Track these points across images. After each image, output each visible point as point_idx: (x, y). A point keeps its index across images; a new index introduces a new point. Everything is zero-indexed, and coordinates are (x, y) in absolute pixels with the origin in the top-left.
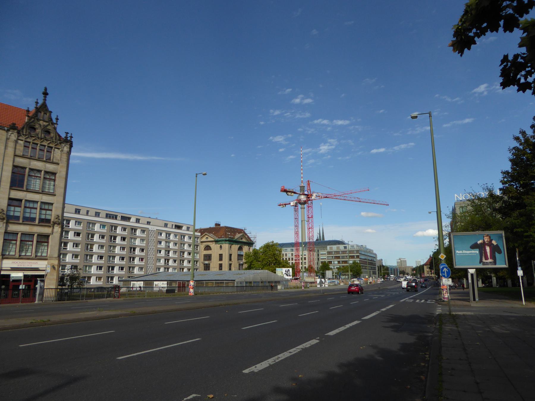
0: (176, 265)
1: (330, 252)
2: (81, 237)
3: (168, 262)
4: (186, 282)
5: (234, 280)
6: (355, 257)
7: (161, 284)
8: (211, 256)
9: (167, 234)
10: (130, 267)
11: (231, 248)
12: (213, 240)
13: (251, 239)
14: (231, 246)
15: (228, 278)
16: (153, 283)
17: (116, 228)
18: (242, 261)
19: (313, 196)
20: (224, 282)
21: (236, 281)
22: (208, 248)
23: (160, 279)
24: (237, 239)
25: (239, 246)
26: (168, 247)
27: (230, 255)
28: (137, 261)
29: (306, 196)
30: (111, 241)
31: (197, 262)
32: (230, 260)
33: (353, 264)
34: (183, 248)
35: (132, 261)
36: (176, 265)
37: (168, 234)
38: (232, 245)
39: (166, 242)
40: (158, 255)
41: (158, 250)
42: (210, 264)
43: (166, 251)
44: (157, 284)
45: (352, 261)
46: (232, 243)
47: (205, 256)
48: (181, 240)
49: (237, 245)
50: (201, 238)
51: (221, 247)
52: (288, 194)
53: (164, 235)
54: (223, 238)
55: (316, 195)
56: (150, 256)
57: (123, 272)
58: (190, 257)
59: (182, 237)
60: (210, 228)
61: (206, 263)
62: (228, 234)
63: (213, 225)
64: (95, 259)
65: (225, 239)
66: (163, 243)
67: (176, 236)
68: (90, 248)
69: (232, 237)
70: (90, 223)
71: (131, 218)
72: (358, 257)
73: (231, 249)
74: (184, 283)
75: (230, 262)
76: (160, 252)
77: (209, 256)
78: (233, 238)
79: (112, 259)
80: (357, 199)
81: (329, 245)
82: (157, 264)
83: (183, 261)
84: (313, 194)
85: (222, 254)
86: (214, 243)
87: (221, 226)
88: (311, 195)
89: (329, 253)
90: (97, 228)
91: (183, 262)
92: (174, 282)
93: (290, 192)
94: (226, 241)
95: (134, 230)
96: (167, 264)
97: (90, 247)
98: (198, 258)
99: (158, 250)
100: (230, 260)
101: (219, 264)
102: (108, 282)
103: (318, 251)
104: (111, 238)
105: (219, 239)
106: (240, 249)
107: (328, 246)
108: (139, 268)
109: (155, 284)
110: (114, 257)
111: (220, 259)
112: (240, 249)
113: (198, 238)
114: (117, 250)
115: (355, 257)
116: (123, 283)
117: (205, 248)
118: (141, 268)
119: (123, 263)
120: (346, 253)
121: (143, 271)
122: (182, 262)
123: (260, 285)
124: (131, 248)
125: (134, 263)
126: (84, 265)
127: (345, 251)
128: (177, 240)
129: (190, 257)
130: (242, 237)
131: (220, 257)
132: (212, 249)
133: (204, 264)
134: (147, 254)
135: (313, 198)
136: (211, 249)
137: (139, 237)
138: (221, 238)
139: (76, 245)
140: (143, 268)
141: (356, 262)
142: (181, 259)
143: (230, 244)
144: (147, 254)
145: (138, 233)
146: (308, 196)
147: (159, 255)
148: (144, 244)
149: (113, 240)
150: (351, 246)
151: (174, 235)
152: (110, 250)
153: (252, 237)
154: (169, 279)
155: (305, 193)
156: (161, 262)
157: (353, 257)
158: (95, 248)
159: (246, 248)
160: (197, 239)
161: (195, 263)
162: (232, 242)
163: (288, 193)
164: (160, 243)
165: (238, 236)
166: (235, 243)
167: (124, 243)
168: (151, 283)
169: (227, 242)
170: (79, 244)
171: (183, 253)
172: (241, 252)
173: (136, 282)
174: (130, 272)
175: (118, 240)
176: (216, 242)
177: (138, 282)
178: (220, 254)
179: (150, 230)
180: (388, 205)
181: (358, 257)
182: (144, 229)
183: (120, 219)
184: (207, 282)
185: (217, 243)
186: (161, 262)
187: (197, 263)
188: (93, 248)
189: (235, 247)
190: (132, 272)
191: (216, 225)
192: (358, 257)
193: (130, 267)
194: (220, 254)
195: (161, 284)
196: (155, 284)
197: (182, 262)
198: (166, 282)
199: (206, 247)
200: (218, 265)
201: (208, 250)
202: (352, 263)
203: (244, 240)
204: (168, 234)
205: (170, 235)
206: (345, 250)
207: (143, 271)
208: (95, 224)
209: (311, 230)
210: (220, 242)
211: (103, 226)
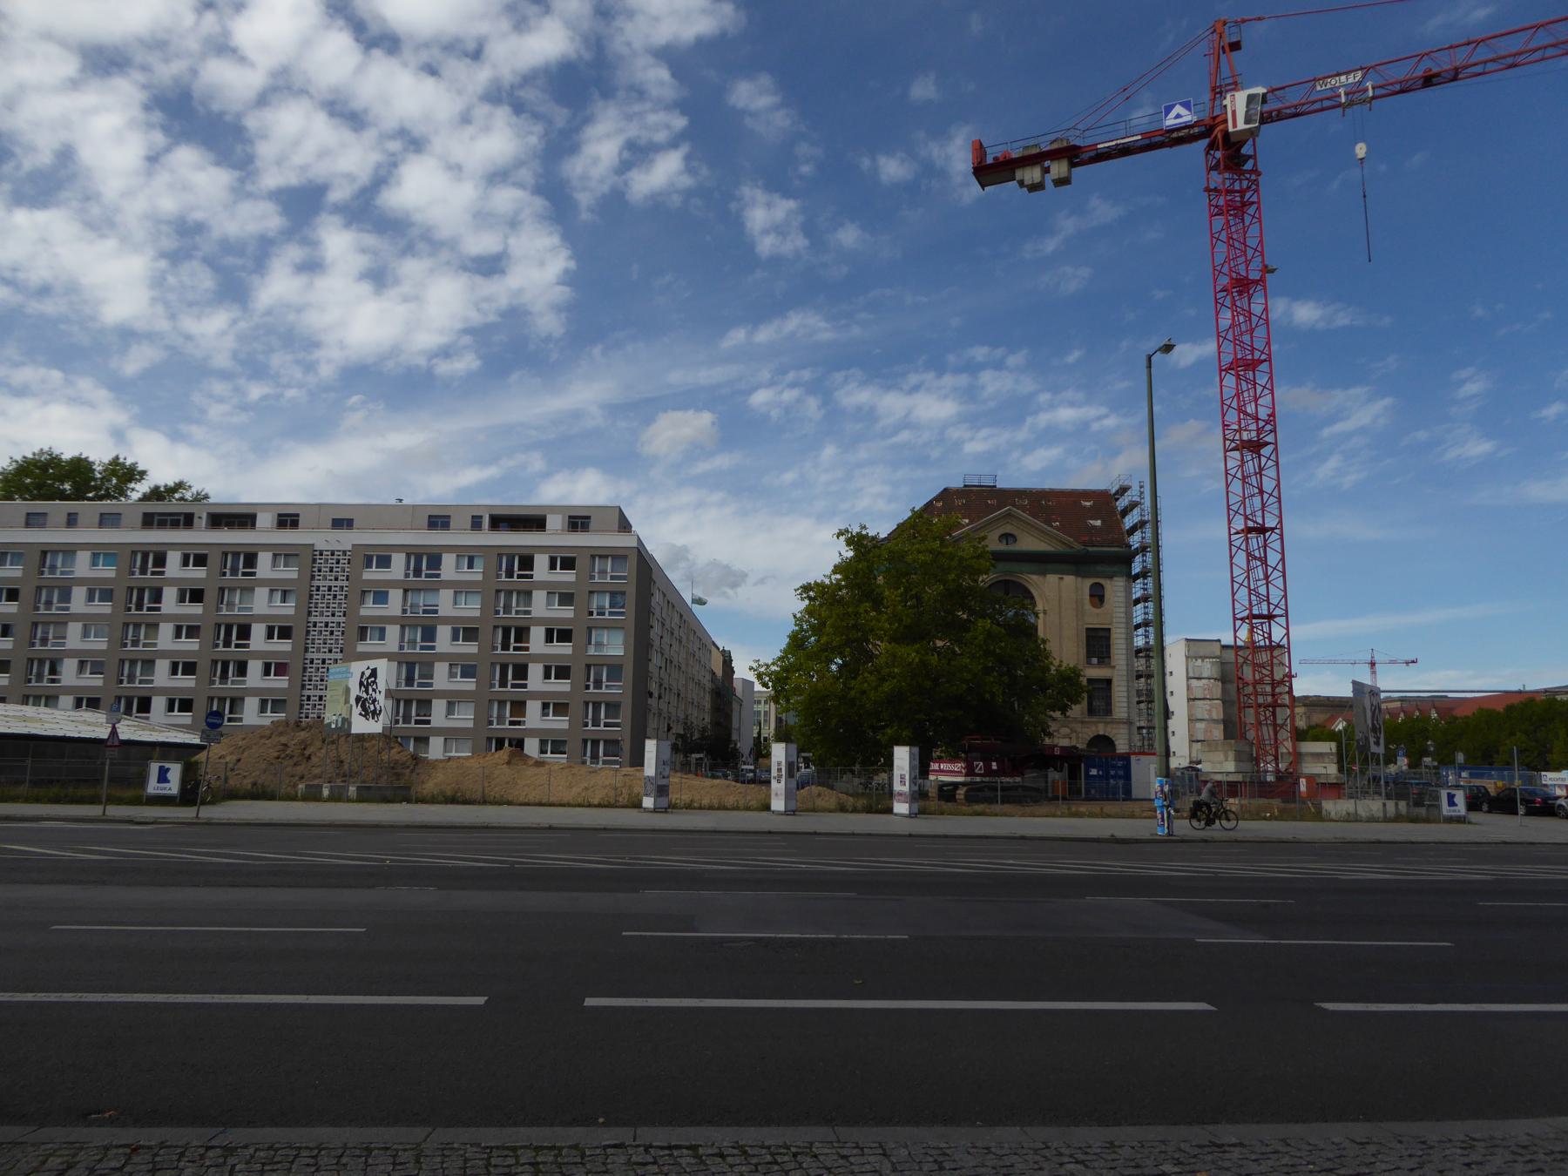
17: (161, 560)
53: (398, 560)
90: (82, 566)
155: (1170, 122)
178: (69, 514)
194: (69, 514)
208: (74, 552)
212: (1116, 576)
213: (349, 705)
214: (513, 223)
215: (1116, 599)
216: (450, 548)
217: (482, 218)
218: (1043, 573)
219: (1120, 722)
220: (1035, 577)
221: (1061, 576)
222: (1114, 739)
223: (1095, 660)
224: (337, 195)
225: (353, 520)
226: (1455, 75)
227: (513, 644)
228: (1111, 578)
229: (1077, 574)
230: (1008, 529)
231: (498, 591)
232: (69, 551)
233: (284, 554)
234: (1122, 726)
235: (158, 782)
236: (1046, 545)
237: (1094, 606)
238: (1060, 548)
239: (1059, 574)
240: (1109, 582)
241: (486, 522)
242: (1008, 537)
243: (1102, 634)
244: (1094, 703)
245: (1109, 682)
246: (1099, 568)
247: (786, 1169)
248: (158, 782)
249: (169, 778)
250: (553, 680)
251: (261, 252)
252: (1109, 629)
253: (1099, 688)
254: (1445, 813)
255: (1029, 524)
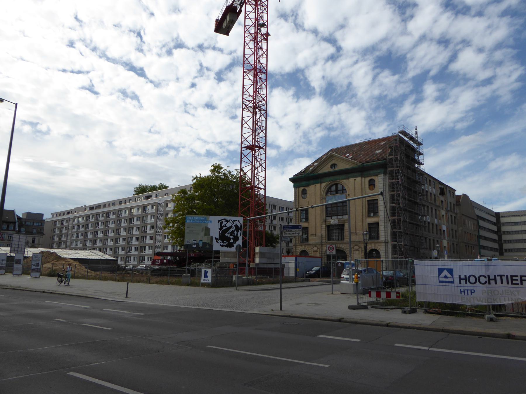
166: (312, 181)
212: (379, 174)
213: (210, 236)
214: (500, 64)
215: (379, 185)
217: (485, 66)
218: (348, 178)
219: (381, 242)
220: (344, 181)
221: (355, 178)
222: (379, 251)
223: (372, 215)
224: (433, 73)
228: (377, 175)
229: (362, 176)
230: (333, 162)
234: (382, 244)
235: (205, 278)
236: (348, 166)
237: (370, 189)
238: (354, 166)
239: (354, 178)
240: (376, 177)
242: (333, 165)
243: (375, 202)
244: (372, 234)
245: (378, 224)
246: (372, 172)
248: (205, 278)
249: (208, 275)
251: (401, 101)
252: (377, 199)
253: (374, 227)
254: (202, 281)
255: (344, 160)
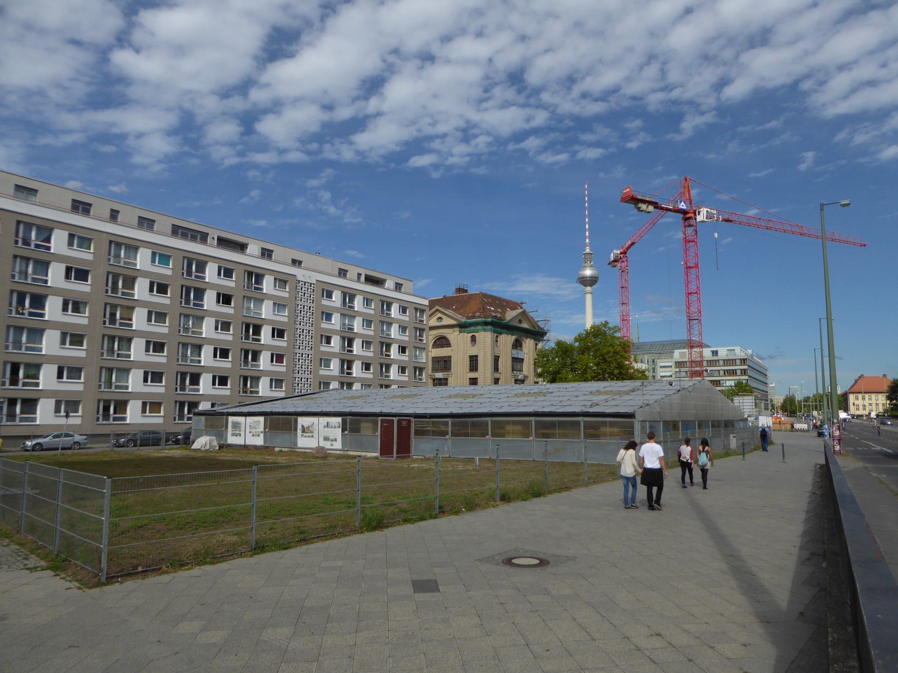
0: (369, 375)
1: (681, 362)
2: (89, 282)
3: (349, 368)
4: (413, 419)
5: (631, 416)
6: (739, 372)
7: (321, 426)
8: (450, 361)
9: (344, 295)
10: (245, 379)
11: (497, 341)
12: (453, 322)
13: (539, 323)
14: (497, 336)
15: (592, 406)
16: (296, 421)
17: (201, 267)
18: (521, 372)
19: (699, 214)
20: (578, 423)
21: (639, 417)
22: (442, 342)
23: (319, 410)
24: (511, 320)
25: (514, 337)
26: (349, 329)
27: (496, 359)
28: (264, 362)
29: (682, 216)
30: (247, 338)
31: (421, 370)
32: (496, 369)
33: (736, 386)
34: (387, 335)
35: (252, 361)
36: (371, 376)
37: (349, 296)
38: (500, 334)
39: (343, 315)
40: (323, 349)
41: (322, 335)
42: (447, 379)
43: (343, 338)
44: (308, 427)
45: (733, 382)
46: (499, 330)
47: (436, 360)
48: (381, 375)
49: (510, 336)
50: (430, 316)
51: (473, 339)
52: (639, 209)
53: (337, 296)
54: (480, 317)
55: (707, 211)
56: (301, 351)
57: (225, 391)
58: (404, 358)
59: (383, 307)
60: (445, 297)
61: (438, 377)
62: (490, 310)
63: (451, 292)
64: (137, 350)
65: (483, 319)
66: (336, 319)
67: (367, 302)
68: (121, 318)
69: (499, 315)
70: (119, 245)
71: (248, 244)
72: (744, 372)
73: (497, 344)
74: (404, 423)
75: (497, 375)
76: (328, 340)
77: (445, 361)
78: (500, 319)
79: (191, 353)
80: (796, 229)
81: (679, 349)
82: (322, 372)
83: (388, 367)
84: (702, 210)
85: (477, 356)
86: (458, 329)
87: (470, 292)
88: (695, 213)
89: (679, 364)
90: (142, 260)
91: (388, 370)
92: (366, 421)
93: (644, 202)
94: (486, 324)
95: (255, 276)
96: (348, 373)
97: (121, 314)
98: (424, 361)
99: (322, 335)
100: (496, 369)
101: (470, 379)
102: (181, 416)
103: (653, 361)
104: (247, 331)
105: (468, 320)
106: (517, 345)
107: (675, 351)
108: (271, 380)
109: (303, 426)
110: (198, 348)
111: (470, 366)
112: (517, 345)
113: (422, 311)
114: (207, 329)
115: (739, 372)
116: (206, 420)
117: (435, 342)
118: (277, 382)
119: (225, 364)
120: (718, 365)
121: (284, 389)
122: (384, 370)
123: (662, 439)
124: (247, 326)
125: (259, 366)
126: (101, 368)
127: (715, 361)
128: (372, 312)
129: (404, 358)
130: (520, 318)
131: (470, 364)
132: (452, 345)
133: (434, 380)
134: (292, 345)
135: (699, 218)
136: (450, 344)
137: (269, 297)
138: (473, 317)
139: (74, 305)
140: (282, 381)
141: (742, 383)
142: (382, 361)
143: (495, 332)
144: (292, 345)
145: (268, 284)
146: (688, 216)
147: (324, 348)
148: (283, 318)
149: (253, 335)
150: (728, 350)
151: (364, 298)
152: (184, 328)
153: (539, 320)
154: (347, 410)
155: (681, 207)
156: (332, 368)
157: (733, 373)
158: (139, 319)
159: (529, 345)
160: (421, 315)
161: (417, 373)
162: (500, 326)
163: (640, 205)
164: (329, 317)
165: (510, 315)
166: (505, 331)
167: (228, 310)
168: (290, 422)
169: (489, 327)
170: (85, 304)
171: (388, 346)
172: (519, 352)
173: (243, 418)
174: (245, 392)
175: (209, 300)
176: (462, 327)
177: (248, 418)
178: (471, 357)
179: (299, 281)
180: (864, 245)
181: (744, 363)
182: (283, 277)
183: (216, 244)
184: (499, 422)
185: (463, 329)
186: (332, 368)
187: (421, 374)
188: (131, 320)
189: (507, 340)
190: (251, 392)
191: (459, 290)
192: (744, 363)
193: (245, 379)
194: (471, 357)
195: (321, 426)
196: (303, 426)
197: (384, 370)
198: (339, 419)
199: (438, 339)
200: (468, 380)
201: (442, 347)
202: (733, 385)
203: (525, 325)
204: (349, 296)
205: (352, 298)
206: (715, 358)
207: (284, 389)
208: (136, 249)
209: (694, 298)
210: (472, 328)
211: (161, 256)
216: (148, 244)
221: (299, 432)
225: (451, 356)
226: (731, 221)
227: (251, 337)
231: (9, 327)
232: (133, 247)
233: (281, 281)
241: (473, 375)
247: (52, 562)
250: (276, 338)
